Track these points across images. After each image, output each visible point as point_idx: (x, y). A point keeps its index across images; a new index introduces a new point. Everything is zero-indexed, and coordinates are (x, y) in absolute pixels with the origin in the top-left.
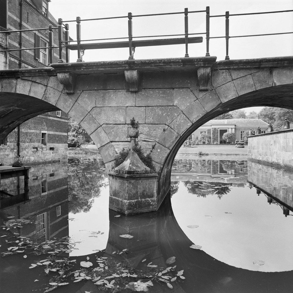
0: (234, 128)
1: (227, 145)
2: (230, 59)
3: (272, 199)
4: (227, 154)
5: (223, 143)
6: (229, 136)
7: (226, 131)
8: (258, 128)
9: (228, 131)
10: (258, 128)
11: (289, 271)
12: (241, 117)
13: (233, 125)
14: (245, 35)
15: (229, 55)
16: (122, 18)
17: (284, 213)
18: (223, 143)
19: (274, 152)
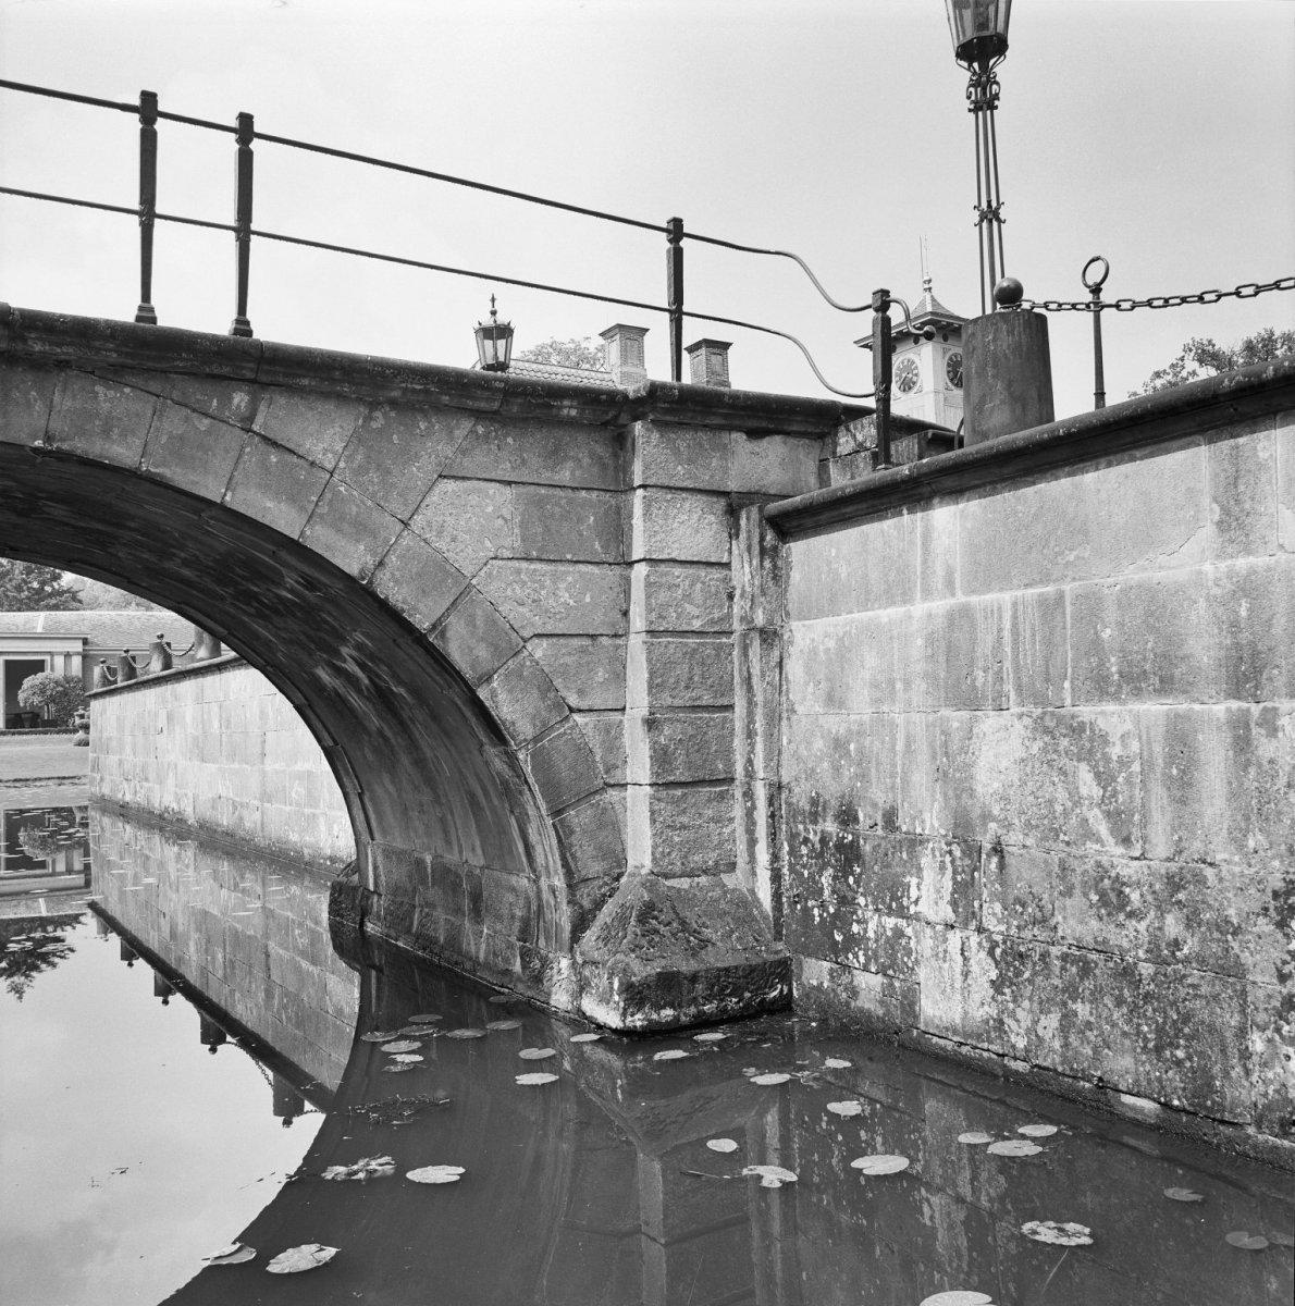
0: (78, 654)
1: (40, 733)
2: (161, 323)
3: (170, 981)
4: (15, 780)
5: (27, 724)
6: (49, 693)
7: (38, 666)
8: (125, 655)
9: (48, 666)
10: (125, 655)
11: (172, 1297)
12: (133, 605)
13: (10, 641)
14: (344, 246)
15: (154, 302)
16: (420, 168)
17: (204, 1040)
18: (27, 724)
19: (169, 764)
